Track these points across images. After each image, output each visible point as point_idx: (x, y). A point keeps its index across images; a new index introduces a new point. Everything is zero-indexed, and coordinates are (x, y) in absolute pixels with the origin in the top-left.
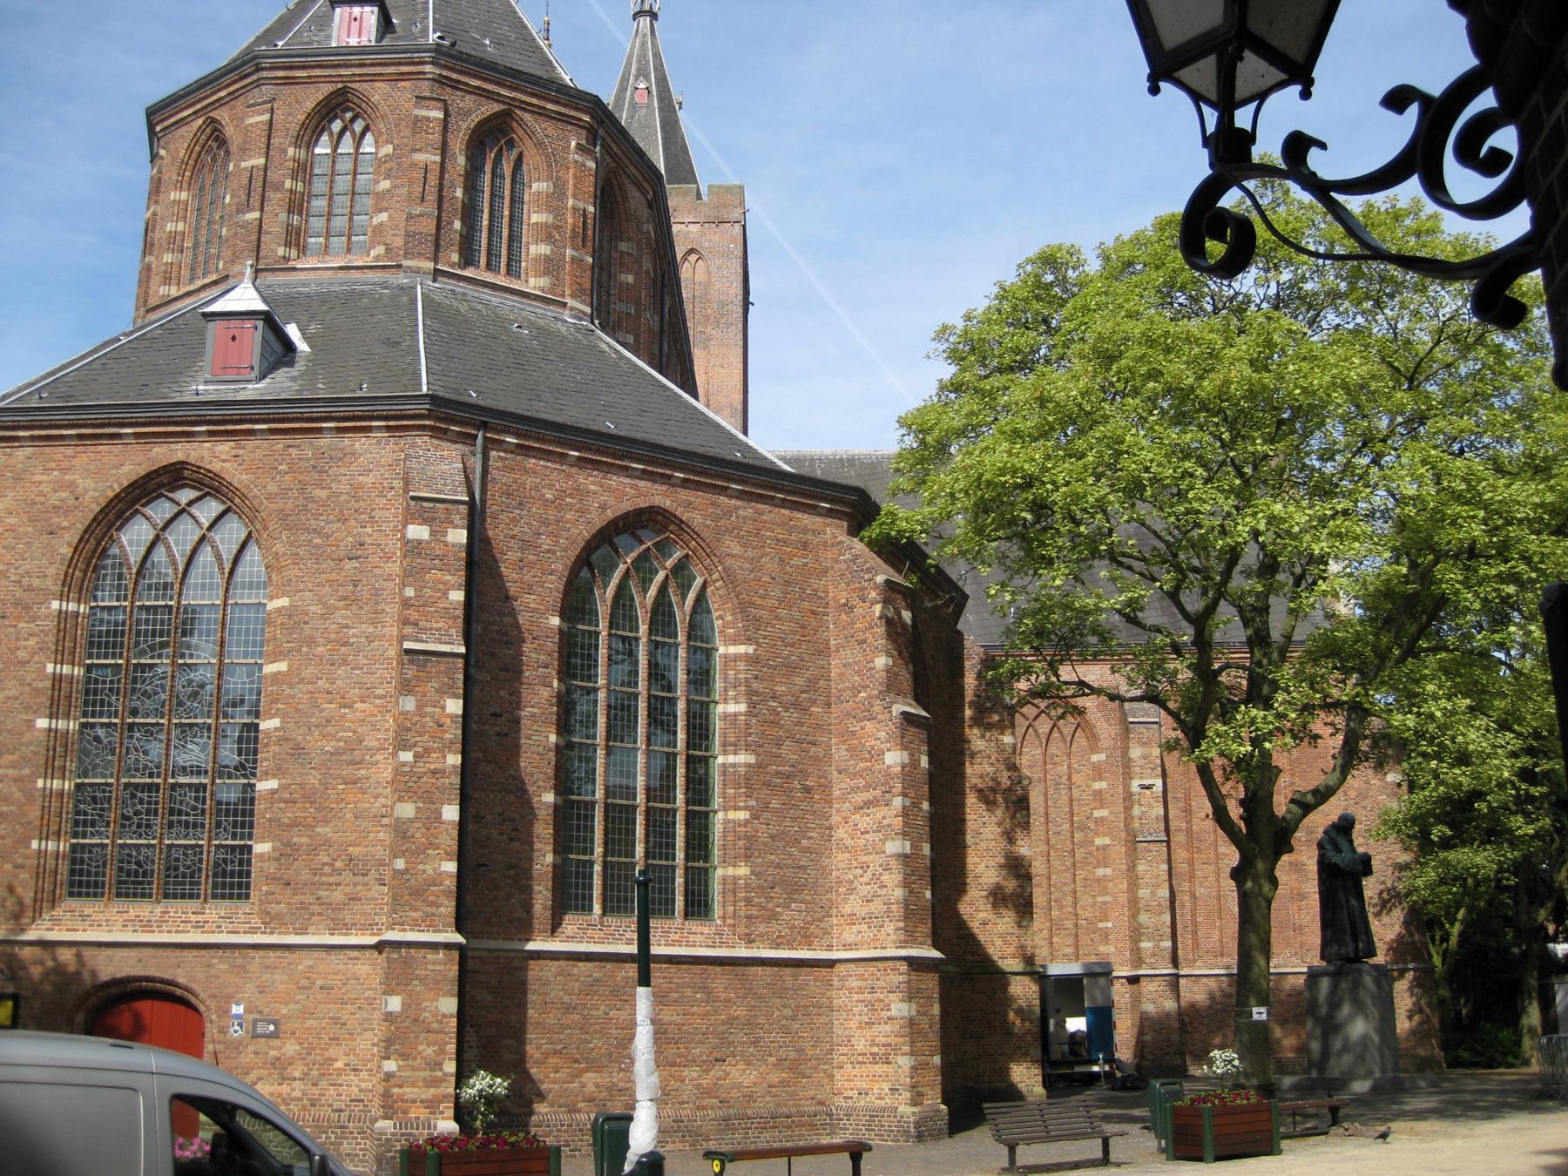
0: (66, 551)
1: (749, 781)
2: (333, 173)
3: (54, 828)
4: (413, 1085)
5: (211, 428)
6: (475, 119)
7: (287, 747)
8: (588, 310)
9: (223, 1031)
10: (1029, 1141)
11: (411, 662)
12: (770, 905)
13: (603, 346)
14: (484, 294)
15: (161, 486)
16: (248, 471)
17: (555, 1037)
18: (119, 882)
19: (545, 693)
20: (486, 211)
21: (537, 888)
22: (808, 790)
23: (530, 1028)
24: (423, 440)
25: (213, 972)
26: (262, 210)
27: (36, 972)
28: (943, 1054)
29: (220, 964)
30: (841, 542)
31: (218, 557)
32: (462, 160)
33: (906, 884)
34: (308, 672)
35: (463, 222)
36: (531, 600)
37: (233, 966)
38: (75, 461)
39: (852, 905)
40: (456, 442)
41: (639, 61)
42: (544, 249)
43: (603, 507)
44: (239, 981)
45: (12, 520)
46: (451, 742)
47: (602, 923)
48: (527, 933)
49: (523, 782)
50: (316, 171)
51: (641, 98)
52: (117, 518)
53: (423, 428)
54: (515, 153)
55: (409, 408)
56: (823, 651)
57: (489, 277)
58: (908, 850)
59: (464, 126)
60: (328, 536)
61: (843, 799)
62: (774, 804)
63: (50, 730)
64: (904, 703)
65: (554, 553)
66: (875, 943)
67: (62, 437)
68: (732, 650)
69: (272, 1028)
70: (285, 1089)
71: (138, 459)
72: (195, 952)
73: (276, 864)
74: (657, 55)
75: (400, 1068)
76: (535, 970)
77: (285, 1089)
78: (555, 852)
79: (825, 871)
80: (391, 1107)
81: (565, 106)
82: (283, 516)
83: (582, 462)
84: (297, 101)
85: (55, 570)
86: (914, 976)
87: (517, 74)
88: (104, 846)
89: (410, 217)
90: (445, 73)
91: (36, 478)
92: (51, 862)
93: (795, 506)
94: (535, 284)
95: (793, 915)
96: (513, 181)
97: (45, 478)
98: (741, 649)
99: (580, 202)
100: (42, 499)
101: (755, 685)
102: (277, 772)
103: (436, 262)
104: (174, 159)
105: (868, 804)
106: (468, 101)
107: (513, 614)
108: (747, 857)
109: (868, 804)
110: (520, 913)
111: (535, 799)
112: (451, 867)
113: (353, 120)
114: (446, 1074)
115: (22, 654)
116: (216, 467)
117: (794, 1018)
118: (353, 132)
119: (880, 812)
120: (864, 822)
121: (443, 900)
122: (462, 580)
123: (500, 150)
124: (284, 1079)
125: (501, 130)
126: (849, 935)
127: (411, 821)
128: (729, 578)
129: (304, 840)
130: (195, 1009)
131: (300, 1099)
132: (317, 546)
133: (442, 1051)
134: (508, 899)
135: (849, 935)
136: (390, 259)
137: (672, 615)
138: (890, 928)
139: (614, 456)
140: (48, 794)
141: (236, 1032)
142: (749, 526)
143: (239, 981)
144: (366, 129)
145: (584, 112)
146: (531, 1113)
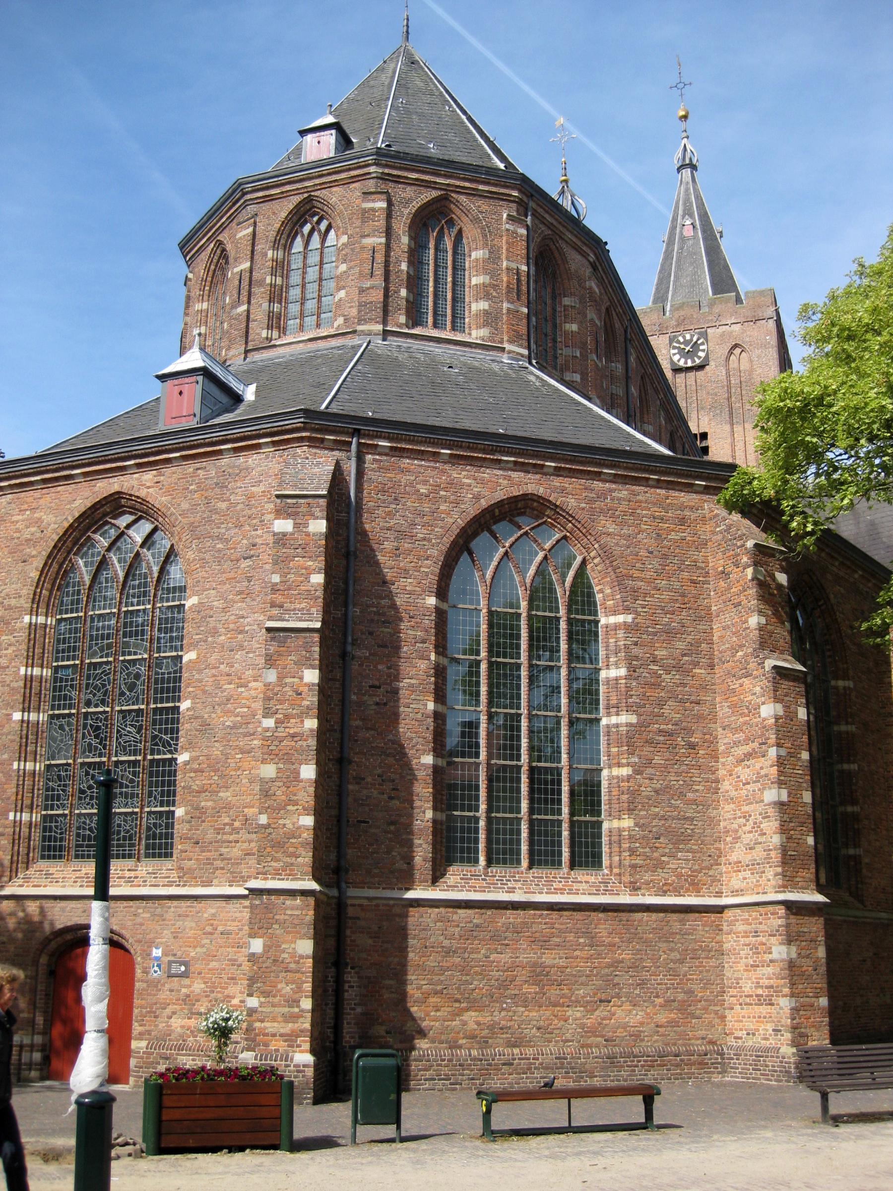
0: (35, 575)
1: (631, 740)
2: (305, 266)
3: (27, 802)
4: (274, 1020)
5: (138, 461)
6: (416, 205)
7: (196, 724)
8: (525, 352)
9: (146, 971)
10: (839, 1089)
11: (273, 639)
13: (532, 378)
14: (429, 348)
15: (105, 514)
16: (168, 493)
17: (436, 978)
18: (77, 846)
19: (423, 665)
20: (431, 279)
21: (417, 842)
22: (692, 746)
23: (411, 970)
24: (302, 451)
25: (139, 920)
26: (249, 303)
27: (11, 923)
28: (831, 998)
29: (143, 911)
30: (717, 515)
32: (405, 240)
33: (783, 829)
34: (213, 658)
35: (409, 289)
36: (408, 583)
37: (154, 915)
38: (42, 502)
39: (738, 854)
40: (332, 450)
41: (685, 204)
42: (483, 305)
43: (477, 498)
44: (158, 928)
46: (308, 707)
47: (486, 874)
48: (407, 880)
49: (402, 747)
50: (293, 267)
51: (688, 232)
52: (74, 544)
53: (301, 439)
54: (455, 231)
55: (288, 423)
56: (707, 616)
57: (436, 333)
58: (784, 797)
59: (406, 211)
60: (227, 541)
61: (727, 753)
62: (657, 760)
63: (23, 721)
64: (777, 659)
66: (757, 888)
67: (31, 483)
68: (612, 620)
69: (183, 968)
70: (192, 1022)
71: (87, 494)
72: (125, 904)
73: (188, 826)
74: (698, 198)
75: (261, 1005)
76: (415, 917)
77: (192, 1022)
78: (435, 809)
79: (713, 822)
80: (254, 1040)
81: (495, 185)
82: (192, 527)
83: (455, 459)
84: (274, 213)
85: (27, 591)
86: (793, 919)
87: (450, 163)
88: (65, 815)
89: (362, 291)
90: (386, 171)
91: (15, 518)
92: (25, 830)
93: (670, 485)
94: (477, 335)
95: (681, 863)
96: (455, 253)
97: (20, 517)
98: (620, 619)
99: (515, 262)
100: (18, 535)
101: (636, 651)
102: (190, 746)
103: (385, 322)
104: (198, 279)
105: (748, 756)
106: (410, 191)
107: (390, 596)
108: (631, 810)
109: (748, 756)
110: (400, 865)
111: (415, 761)
112: (308, 821)
113: (319, 222)
114: (302, 1011)
116: (142, 493)
117: (682, 961)
118: (320, 231)
119: (757, 763)
120: (744, 773)
121: (301, 851)
122: (322, 565)
123: (442, 228)
125: (441, 213)
126: (736, 882)
127: (273, 780)
128: (607, 554)
129: (209, 804)
130: (127, 950)
132: (219, 551)
133: (299, 989)
135: (736, 882)
136: (348, 327)
137: (552, 590)
138: (770, 873)
139: (484, 451)
140: (856, 845)
141: (156, 973)
142: (624, 506)
143: (158, 928)
144: (329, 227)
145: (513, 189)
146: (413, 1048)
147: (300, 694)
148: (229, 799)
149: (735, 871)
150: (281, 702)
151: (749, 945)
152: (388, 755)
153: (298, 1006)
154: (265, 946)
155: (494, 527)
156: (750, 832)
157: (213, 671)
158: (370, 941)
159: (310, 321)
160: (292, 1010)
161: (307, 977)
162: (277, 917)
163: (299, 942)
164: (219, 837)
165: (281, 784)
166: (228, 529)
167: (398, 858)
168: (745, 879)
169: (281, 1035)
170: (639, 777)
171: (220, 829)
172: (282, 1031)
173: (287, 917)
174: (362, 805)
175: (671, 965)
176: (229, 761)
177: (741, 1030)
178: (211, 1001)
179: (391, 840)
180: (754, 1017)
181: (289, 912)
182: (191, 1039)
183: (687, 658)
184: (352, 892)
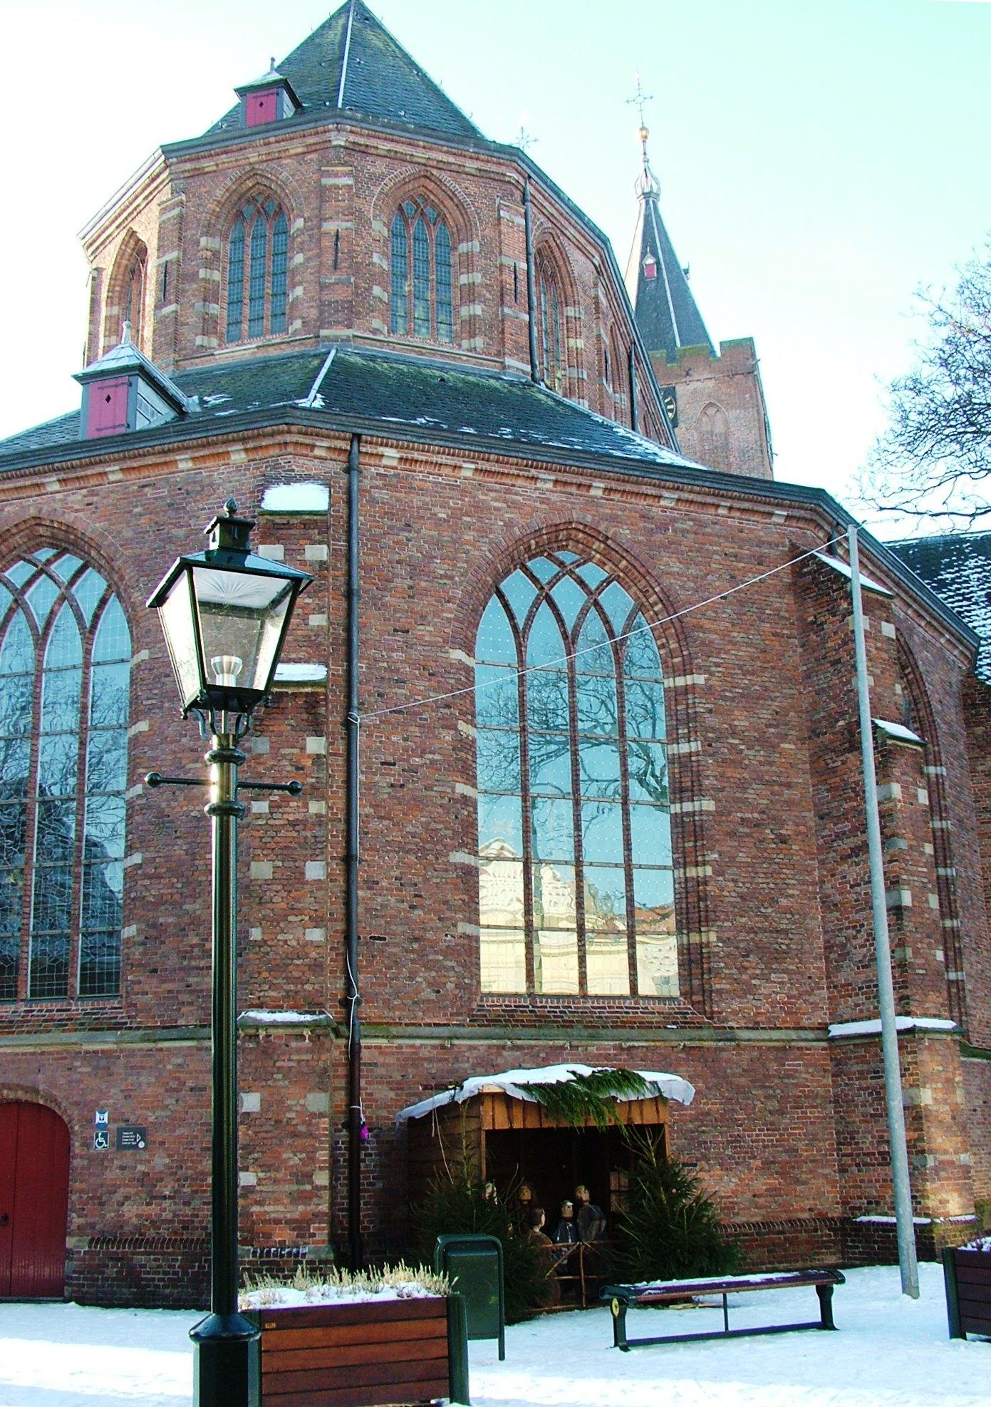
4: (277, 1201)
6: (388, 183)
7: (150, 816)
9: (86, 1144)
12: (744, 977)
22: (783, 840)
31: (79, 617)
37: (96, 1068)
43: (509, 525)
62: (742, 857)
65: (452, 578)
70: (153, 1210)
77: (153, 1210)
106: (380, 167)
114: (318, 1188)
116: (69, 518)
117: (782, 1112)
124: (154, 1198)
134: (411, 978)
147: (302, 769)
148: (198, 912)
149: (843, 996)
151: (867, 1088)
152: (407, 852)
153: (311, 1183)
155: (529, 564)
156: (862, 946)
158: (392, 1094)
160: (302, 1188)
161: (321, 1142)
162: (278, 1064)
163: (310, 1096)
164: (185, 963)
165: (280, 887)
167: (424, 985)
168: (857, 1005)
169: (288, 1222)
170: (721, 878)
171: (187, 952)
173: (291, 1064)
174: (376, 916)
175: (769, 1118)
176: (197, 862)
177: (859, 1198)
178: (178, 1180)
179: (413, 961)
180: (877, 1181)
181: (295, 1057)
183: (772, 730)
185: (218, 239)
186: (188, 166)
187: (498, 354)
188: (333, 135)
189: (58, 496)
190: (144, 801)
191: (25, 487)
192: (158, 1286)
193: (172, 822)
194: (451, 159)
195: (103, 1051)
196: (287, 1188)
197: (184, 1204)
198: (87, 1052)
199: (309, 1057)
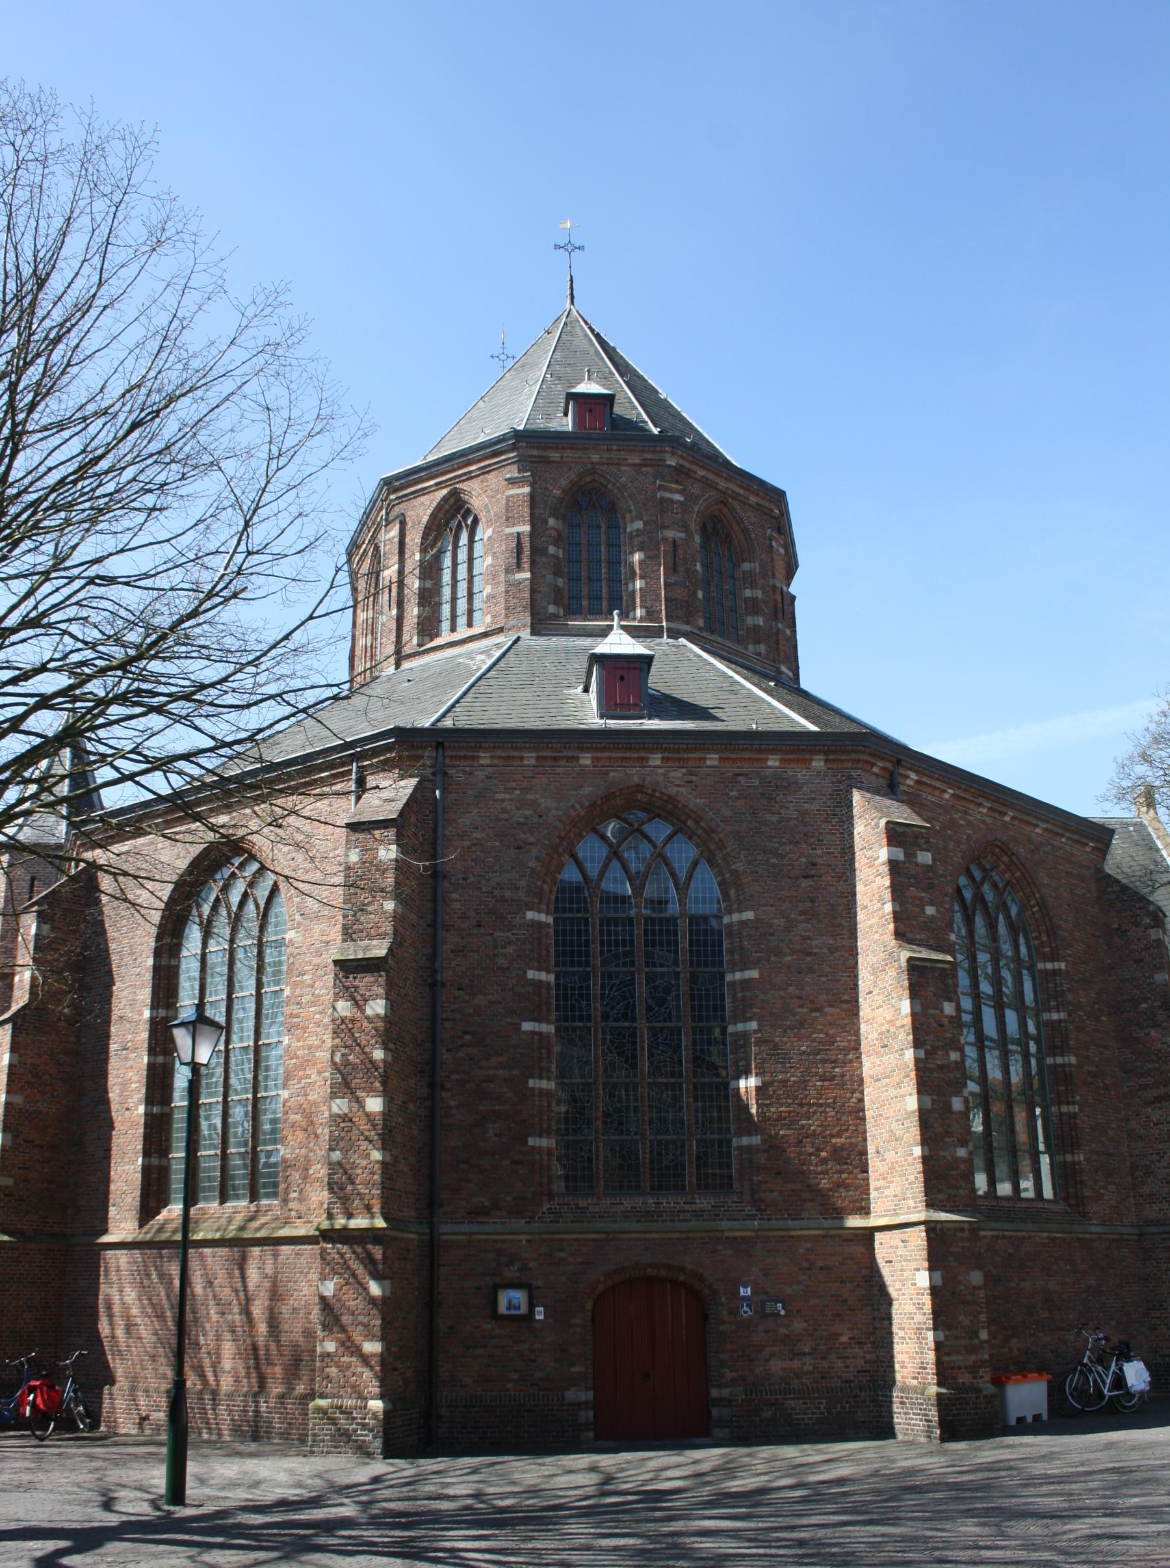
9: (734, 1312)
38: (535, 781)
45: (477, 835)
60: (782, 857)
65: (945, 877)
70: (796, 1364)
77: (796, 1364)
91: (499, 796)
97: (508, 796)
113: (465, 518)
115: (501, 961)
116: (673, 790)
124: (795, 1355)
131: (812, 1373)
132: (774, 866)
141: (746, 1312)
150: (927, 1034)
153: (978, 1337)
154: (943, 1278)
157: (782, 993)
159: (462, 621)
166: (781, 844)
169: (966, 1368)
172: (967, 1363)
181: (960, 1244)
182: (796, 1381)
184: (444, 1228)
185: (560, 522)
186: (535, 452)
187: (774, 661)
188: (667, 456)
189: (660, 771)
190: (759, 1035)
191: (630, 758)
192: (808, 1424)
193: (786, 1054)
194: (741, 492)
195: (742, 1238)
196: (963, 1342)
197: (822, 1358)
198: (727, 1238)
199: (967, 1244)
